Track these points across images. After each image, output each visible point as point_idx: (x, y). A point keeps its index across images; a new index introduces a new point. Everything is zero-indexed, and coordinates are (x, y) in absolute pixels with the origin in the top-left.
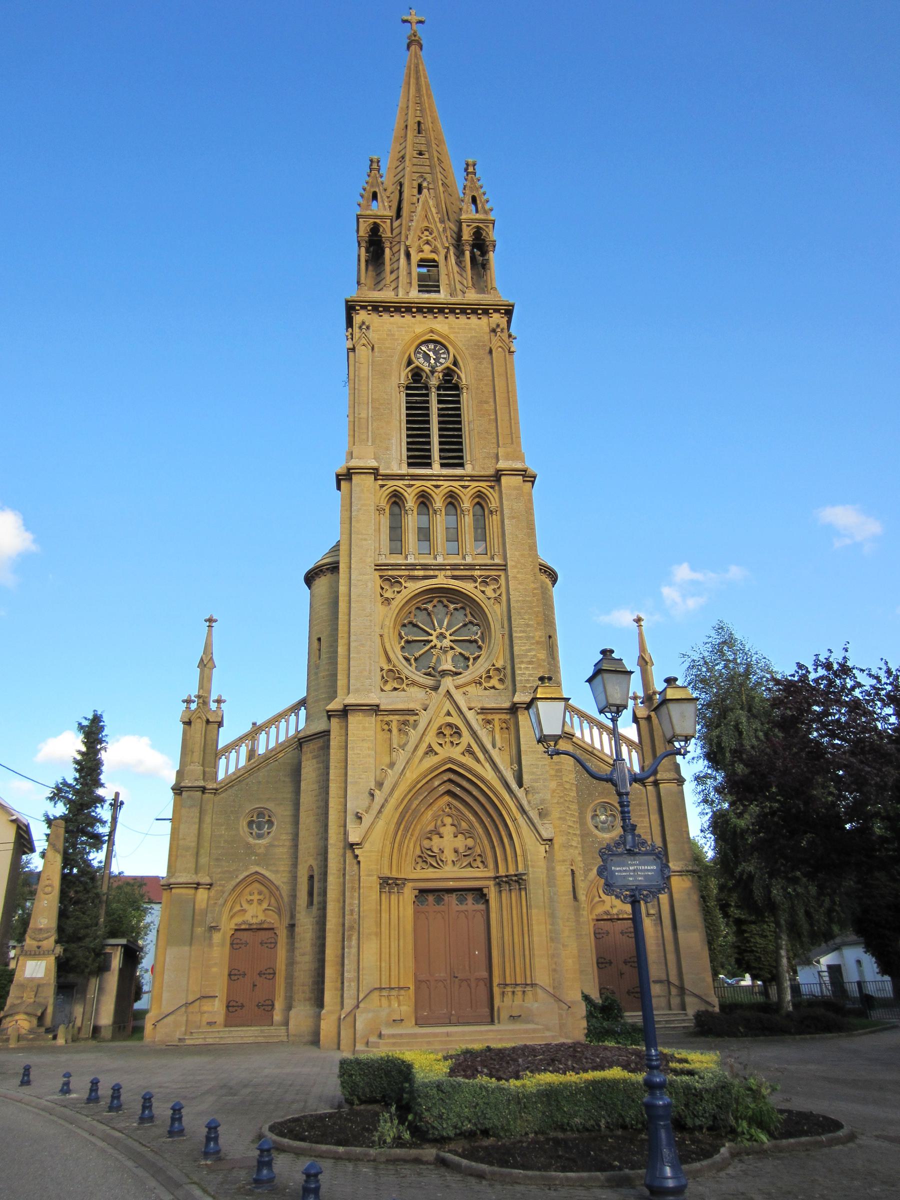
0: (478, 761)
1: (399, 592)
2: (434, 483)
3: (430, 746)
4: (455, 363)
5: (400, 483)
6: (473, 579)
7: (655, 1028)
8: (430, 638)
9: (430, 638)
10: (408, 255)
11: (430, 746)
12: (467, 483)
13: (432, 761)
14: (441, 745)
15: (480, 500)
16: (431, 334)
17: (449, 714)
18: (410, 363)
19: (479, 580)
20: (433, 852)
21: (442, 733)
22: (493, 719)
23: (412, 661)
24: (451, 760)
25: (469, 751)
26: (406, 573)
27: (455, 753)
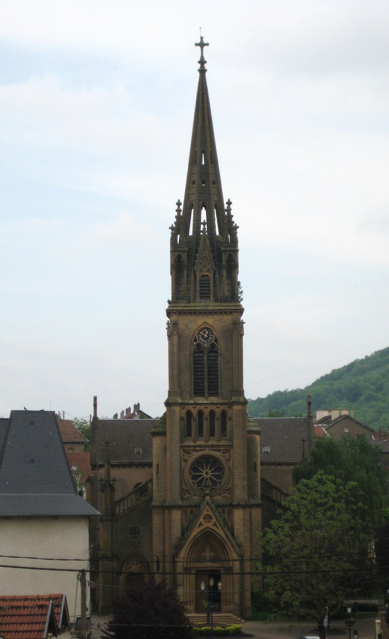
0: (217, 527)
1: (190, 457)
2: (205, 406)
3: (201, 523)
4: (216, 340)
5: (191, 407)
6: (219, 451)
7: (375, 622)
8: (202, 474)
9: (202, 474)
10: (195, 275)
11: (201, 523)
12: (219, 406)
13: (202, 528)
14: (205, 522)
15: (224, 414)
16: (206, 324)
17: (208, 510)
18: (195, 340)
19: (222, 451)
20: (202, 557)
21: (205, 517)
22: (225, 510)
23: (196, 484)
24: (208, 528)
25: (215, 524)
26: (193, 449)
27: (210, 525)
